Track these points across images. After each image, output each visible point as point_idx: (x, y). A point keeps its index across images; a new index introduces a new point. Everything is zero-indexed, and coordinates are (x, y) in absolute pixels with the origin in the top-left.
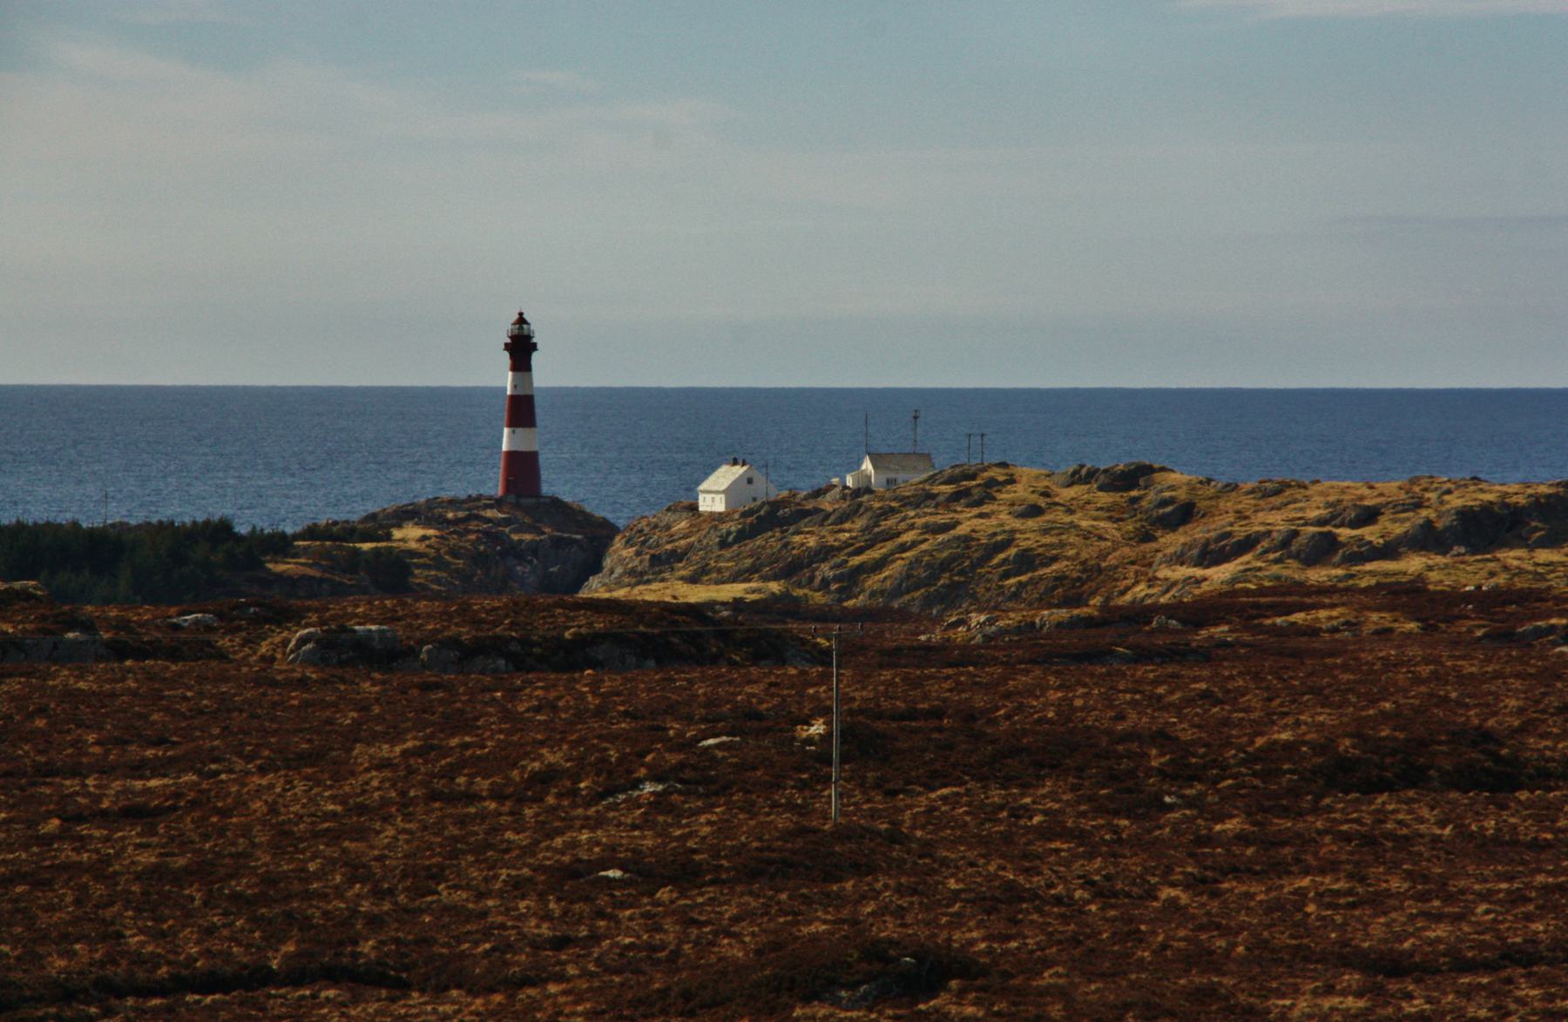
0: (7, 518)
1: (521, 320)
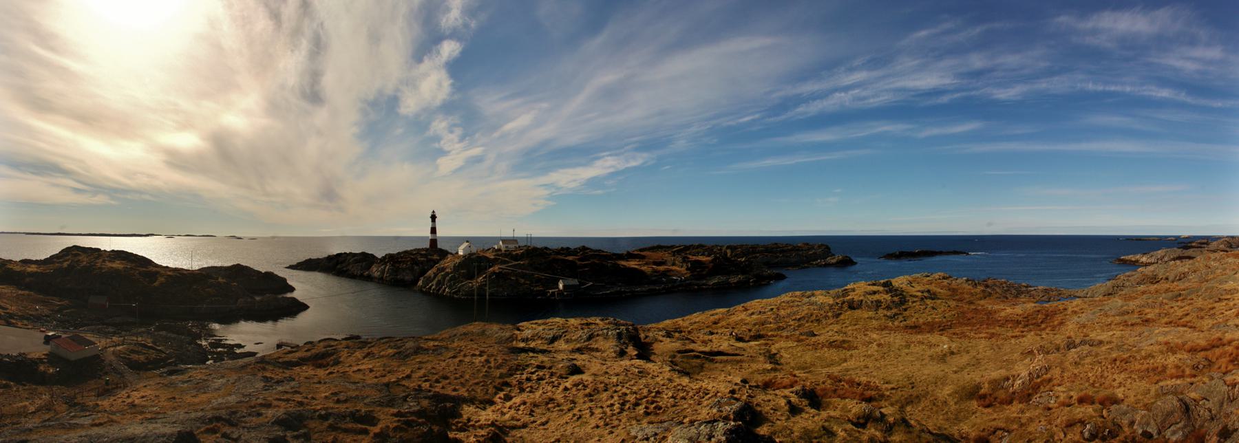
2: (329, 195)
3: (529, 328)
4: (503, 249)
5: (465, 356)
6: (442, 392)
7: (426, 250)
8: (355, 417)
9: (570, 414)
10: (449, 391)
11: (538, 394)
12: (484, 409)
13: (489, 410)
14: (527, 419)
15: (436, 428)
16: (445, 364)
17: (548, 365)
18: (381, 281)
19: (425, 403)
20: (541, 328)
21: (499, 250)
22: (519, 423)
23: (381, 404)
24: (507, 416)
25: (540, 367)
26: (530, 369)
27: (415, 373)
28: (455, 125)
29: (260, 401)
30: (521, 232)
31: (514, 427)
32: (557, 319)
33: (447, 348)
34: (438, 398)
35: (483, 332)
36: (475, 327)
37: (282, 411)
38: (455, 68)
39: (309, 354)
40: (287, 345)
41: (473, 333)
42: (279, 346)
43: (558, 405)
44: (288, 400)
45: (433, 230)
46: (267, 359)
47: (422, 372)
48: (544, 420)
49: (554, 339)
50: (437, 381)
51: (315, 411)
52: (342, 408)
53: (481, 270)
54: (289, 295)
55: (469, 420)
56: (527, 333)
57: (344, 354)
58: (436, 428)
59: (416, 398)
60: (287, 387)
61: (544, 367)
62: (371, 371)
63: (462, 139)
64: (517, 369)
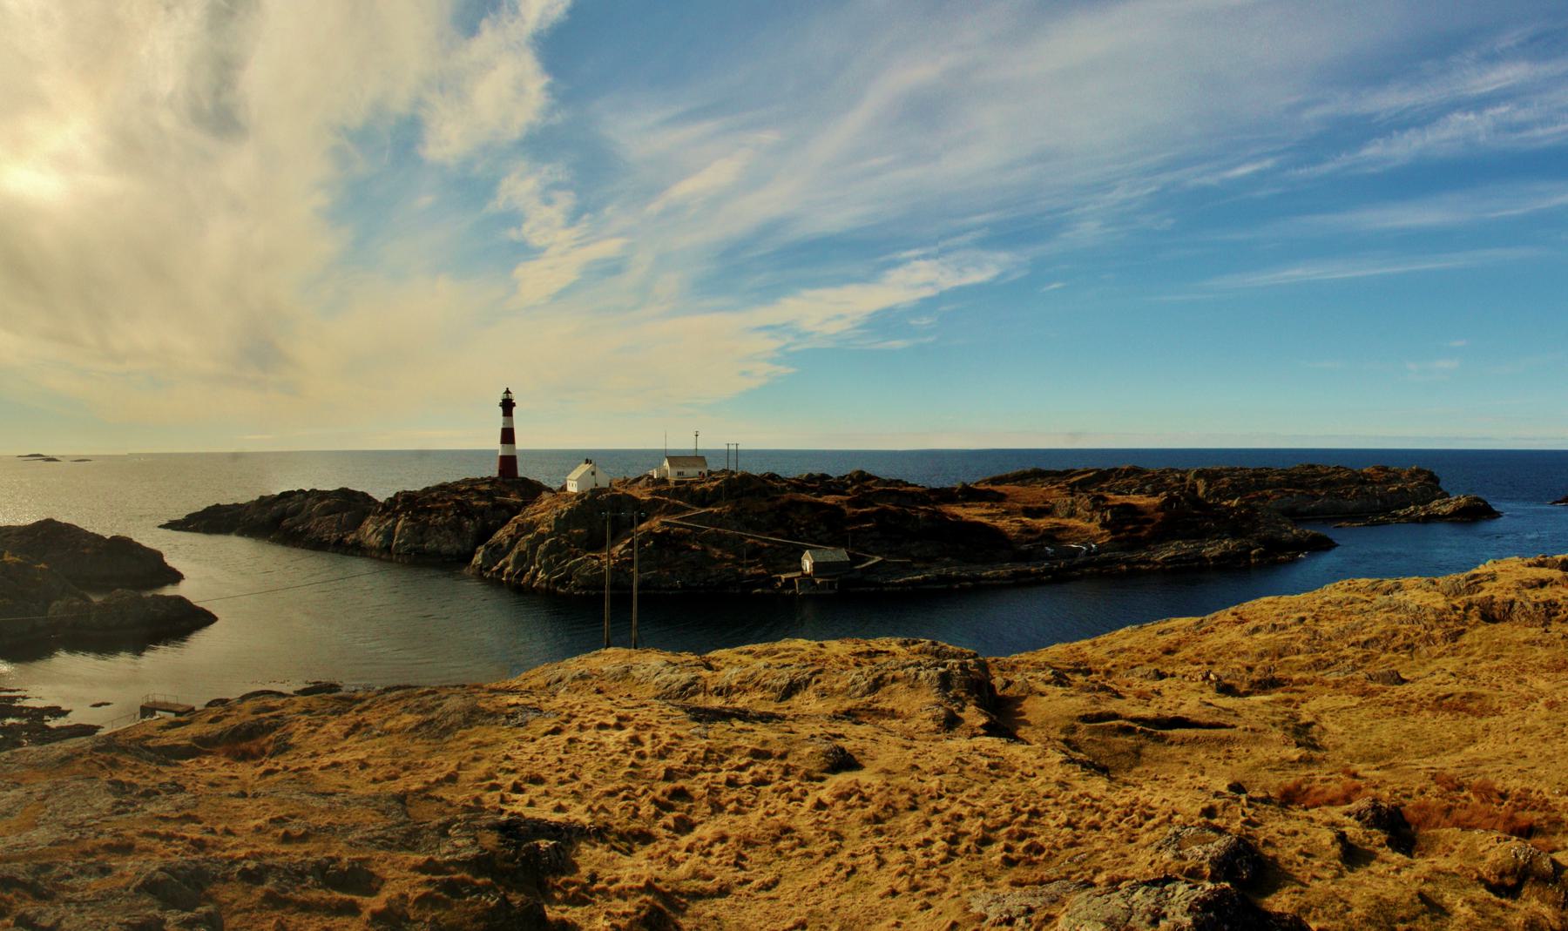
1: (508, 392)
2: (261, 354)
3: (734, 664)
5: (582, 728)
6: (529, 813)
8: (328, 874)
9: (830, 864)
10: (545, 812)
11: (755, 816)
12: (630, 852)
13: (641, 854)
14: (728, 875)
15: (517, 899)
17: (778, 750)
18: (384, 554)
21: (664, 481)
22: (710, 886)
23: (387, 844)
24: (683, 870)
25: (759, 755)
26: (736, 760)
28: (557, 186)
29: (106, 839)
31: (698, 895)
32: (800, 643)
36: (608, 660)
39: (217, 728)
40: (166, 708)
41: (601, 675)
43: (802, 844)
44: (169, 837)
45: (508, 436)
46: (121, 740)
47: (485, 765)
48: (768, 877)
49: (791, 690)
50: (517, 788)
51: (233, 861)
52: (297, 853)
53: (620, 529)
54: (169, 591)
55: (594, 878)
56: (730, 675)
57: (299, 729)
58: (517, 899)
61: (767, 755)
62: (364, 765)
63: (574, 217)
64: (706, 760)
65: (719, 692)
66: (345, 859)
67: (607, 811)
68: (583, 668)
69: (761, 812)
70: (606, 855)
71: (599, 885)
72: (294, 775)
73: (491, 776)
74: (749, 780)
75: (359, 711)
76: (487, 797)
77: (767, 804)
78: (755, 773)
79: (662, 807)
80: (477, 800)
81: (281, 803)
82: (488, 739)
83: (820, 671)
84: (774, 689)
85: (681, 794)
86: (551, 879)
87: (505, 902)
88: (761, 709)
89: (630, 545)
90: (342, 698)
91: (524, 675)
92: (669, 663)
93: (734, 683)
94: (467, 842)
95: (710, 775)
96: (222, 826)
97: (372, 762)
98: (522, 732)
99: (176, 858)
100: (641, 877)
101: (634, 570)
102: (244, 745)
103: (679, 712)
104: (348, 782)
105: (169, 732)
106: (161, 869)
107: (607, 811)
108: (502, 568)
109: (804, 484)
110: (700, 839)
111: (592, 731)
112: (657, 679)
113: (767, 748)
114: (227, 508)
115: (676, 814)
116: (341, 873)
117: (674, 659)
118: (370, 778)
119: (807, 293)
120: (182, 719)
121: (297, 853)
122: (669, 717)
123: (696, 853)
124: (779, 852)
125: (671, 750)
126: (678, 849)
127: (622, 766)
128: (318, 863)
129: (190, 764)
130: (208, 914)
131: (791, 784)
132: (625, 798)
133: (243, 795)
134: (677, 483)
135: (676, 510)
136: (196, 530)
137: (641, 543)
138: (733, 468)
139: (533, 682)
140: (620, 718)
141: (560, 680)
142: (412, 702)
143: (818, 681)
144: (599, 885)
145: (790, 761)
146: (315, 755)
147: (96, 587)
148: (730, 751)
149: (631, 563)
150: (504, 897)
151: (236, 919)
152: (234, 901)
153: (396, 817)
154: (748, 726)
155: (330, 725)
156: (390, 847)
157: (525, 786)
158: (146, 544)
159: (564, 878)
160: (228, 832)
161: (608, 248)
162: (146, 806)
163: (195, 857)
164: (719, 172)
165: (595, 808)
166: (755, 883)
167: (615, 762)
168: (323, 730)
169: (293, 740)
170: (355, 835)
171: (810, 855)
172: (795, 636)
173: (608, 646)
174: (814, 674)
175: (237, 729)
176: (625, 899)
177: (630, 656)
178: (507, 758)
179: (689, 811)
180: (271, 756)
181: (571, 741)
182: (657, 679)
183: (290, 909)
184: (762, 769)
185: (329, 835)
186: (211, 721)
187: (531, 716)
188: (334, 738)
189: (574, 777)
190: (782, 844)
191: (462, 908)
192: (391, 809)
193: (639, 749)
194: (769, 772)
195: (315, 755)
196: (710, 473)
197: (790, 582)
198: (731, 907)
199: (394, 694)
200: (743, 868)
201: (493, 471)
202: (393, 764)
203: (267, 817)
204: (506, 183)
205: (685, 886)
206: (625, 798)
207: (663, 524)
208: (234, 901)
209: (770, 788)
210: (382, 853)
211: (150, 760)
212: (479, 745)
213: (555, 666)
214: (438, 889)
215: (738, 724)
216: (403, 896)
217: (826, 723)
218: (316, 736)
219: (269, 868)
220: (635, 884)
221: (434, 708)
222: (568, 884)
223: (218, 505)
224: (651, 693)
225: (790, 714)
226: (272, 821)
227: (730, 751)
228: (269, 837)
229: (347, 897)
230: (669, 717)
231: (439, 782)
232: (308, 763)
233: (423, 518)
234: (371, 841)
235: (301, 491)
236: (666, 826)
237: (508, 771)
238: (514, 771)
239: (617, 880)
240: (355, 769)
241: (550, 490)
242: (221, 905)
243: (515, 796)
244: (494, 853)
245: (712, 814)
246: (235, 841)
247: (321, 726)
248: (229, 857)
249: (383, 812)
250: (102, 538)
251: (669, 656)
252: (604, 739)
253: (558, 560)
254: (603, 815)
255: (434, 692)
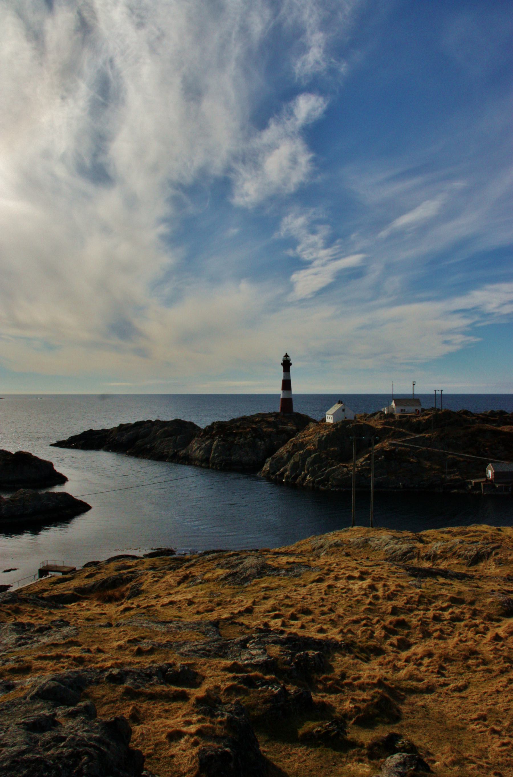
0: (1, 449)
1: (286, 356)
2: (122, 328)
3: (438, 540)
4: (397, 412)
5: (337, 578)
6: (301, 633)
7: (276, 415)
8: (166, 675)
9: (504, 679)
10: (312, 633)
11: (452, 642)
12: (367, 660)
13: (375, 663)
14: (433, 678)
15: (292, 689)
16: (305, 591)
17: (469, 599)
18: (205, 464)
19: (275, 650)
20: (457, 540)
21: (391, 415)
22: (421, 685)
23: (206, 654)
24: (402, 673)
25: (456, 601)
26: (439, 603)
27: (259, 605)
28: (320, 222)
29: (11, 665)
30: (428, 384)
31: (413, 691)
32: (484, 527)
33: (308, 566)
34: (295, 643)
35: (366, 542)
36: (353, 534)
37: (49, 675)
38: (315, 135)
39: (91, 581)
40: (55, 569)
41: (349, 544)
42: (43, 572)
43: (485, 662)
44: (58, 657)
45: (287, 385)
46: (23, 595)
47: (271, 602)
48: (460, 683)
49: (478, 559)
50: (294, 617)
51: (103, 670)
52: (146, 662)
53: (362, 447)
54: (57, 489)
55: (343, 676)
56: (436, 547)
57: (148, 579)
58: (292, 689)
59: (260, 642)
60: (57, 637)
61: (461, 601)
62: (190, 603)
63: (329, 243)
64: (420, 602)
65: (428, 558)
66: (179, 664)
67: (353, 633)
68: (337, 539)
69: (456, 639)
70: (351, 661)
71: (347, 681)
72: (144, 611)
73: (274, 609)
74: (448, 617)
75: (187, 567)
76: (272, 623)
77: (460, 634)
78: (453, 613)
79: (390, 632)
80: (266, 624)
81: (135, 629)
82: (273, 585)
83: (498, 547)
84: (466, 558)
85: (402, 624)
86: (316, 676)
87: (284, 692)
88: (456, 571)
89: (369, 459)
90: (176, 559)
91: (297, 543)
92: (394, 537)
93: (438, 552)
94: (259, 652)
95: (422, 612)
96: (95, 647)
97: (196, 600)
98: (297, 581)
99: (63, 671)
100: (375, 677)
101: (372, 475)
102: (110, 592)
103: (402, 570)
104: (180, 614)
105: (58, 585)
106: (53, 679)
107: (353, 633)
108: (283, 474)
109: (487, 418)
110: (415, 654)
111: (343, 581)
112: (386, 548)
113: (461, 597)
114: (97, 432)
115: (399, 637)
116: (176, 673)
117: (398, 535)
118: (195, 611)
119: (490, 287)
120: (67, 576)
121: (146, 662)
122: (394, 573)
123: (412, 663)
124: (468, 667)
125: (396, 595)
126: (400, 660)
127: (363, 604)
128: (160, 668)
129: (73, 607)
130: (86, 707)
131: (477, 622)
132: (365, 625)
133: (110, 625)
134: (400, 417)
135: (401, 435)
136: (76, 447)
137: (376, 457)
138: (438, 406)
139: (304, 548)
140: (362, 573)
141: (321, 547)
142: (223, 561)
143: (497, 554)
144: (347, 681)
145: (477, 606)
146: (158, 596)
147: (1, 490)
148: (436, 597)
149: (369, 470)
150: (283, 688)
151: (105, 708)
152: (104, 696)
153: (212, 636)
154: (448, 581)
155: (168, 577)
156: (208, 656)
157: (299, 615)
158: (41, 457)
159: (324, 676)
160: (99, 651)
161: (352, 260)
162: (40, 639)
163: (77, 669)
164: (426, 210)
165: (345, 631)
166: (452, 685)
167: (358, 601)
168: (163, 580)
169: (143, 587)
170: (185, 649)
171: (490, 671)
172: (479, 522)
173: (353, 525)
174: (494, 549)
175: (105, 582)
176: (364, 690)
177: (368, 532)
178: (287, 597)
179: (408, 635)
180: (129, 598)
181: (330, 587)
182: (386, 548)
183: (142, 699)
184: (457, 611)
185: (167, 649)
186: (87, 577)
187: (303, 570)
188: (171, 585)
189: (331, 610)
190: (470, 662)
191: (256, 694)
192: (208, 631)
193: (375, 593)
194: (462, 613)
195: (158, 596)
196: (423, 410)
197: (478, 484)
198: (435, 701)
199: (210, 556)
200: (443, 675)
201: (277, 408)
202: (210, 601)
203: (126, 639)
204: (287, 220)
205: (404, 684)
206: (365, 625)
207: (391, 444)
208: (104, 696)
209: (462, 623)
210: (203, 660)
211: (44, 606)
212: (267, 589)
213: (318, 537)
214: (240, 682)
215: (442, 580)
216: (217, 687)
217: (502, 583)
218: (159, 585)
219: (127, 673)
220: (371, 681)
221: (237, 565)
222: (327, 679)
223: (91, 430)
224: (382, 556)
225: (477, 575)
226: (129, 641)
227: (436, 597)
228: (127, 652)
229: (180, 689)
230: (394, 573)
231: (240, 613)
232: (153, 602)
233: (230, 439)
234: (196, 652)
235: (149, 421)
236: (392, 645)
237: (288, 606)
238: (292, 606)
239: (359, 678)
240: (185, 605)
241: (314, 421)
242: (95, 699)
243: (292, 622)
244: (277, 659)
245: (423, 638)
246: (104, 656)
247: (162, 577)
248: (100, 667)
249: (203, 633)
250: (10, 453)
251: (393, 533)
252: (351, 586)
253: (320, 468)
254: (350, 635)
255: (237, 555)
